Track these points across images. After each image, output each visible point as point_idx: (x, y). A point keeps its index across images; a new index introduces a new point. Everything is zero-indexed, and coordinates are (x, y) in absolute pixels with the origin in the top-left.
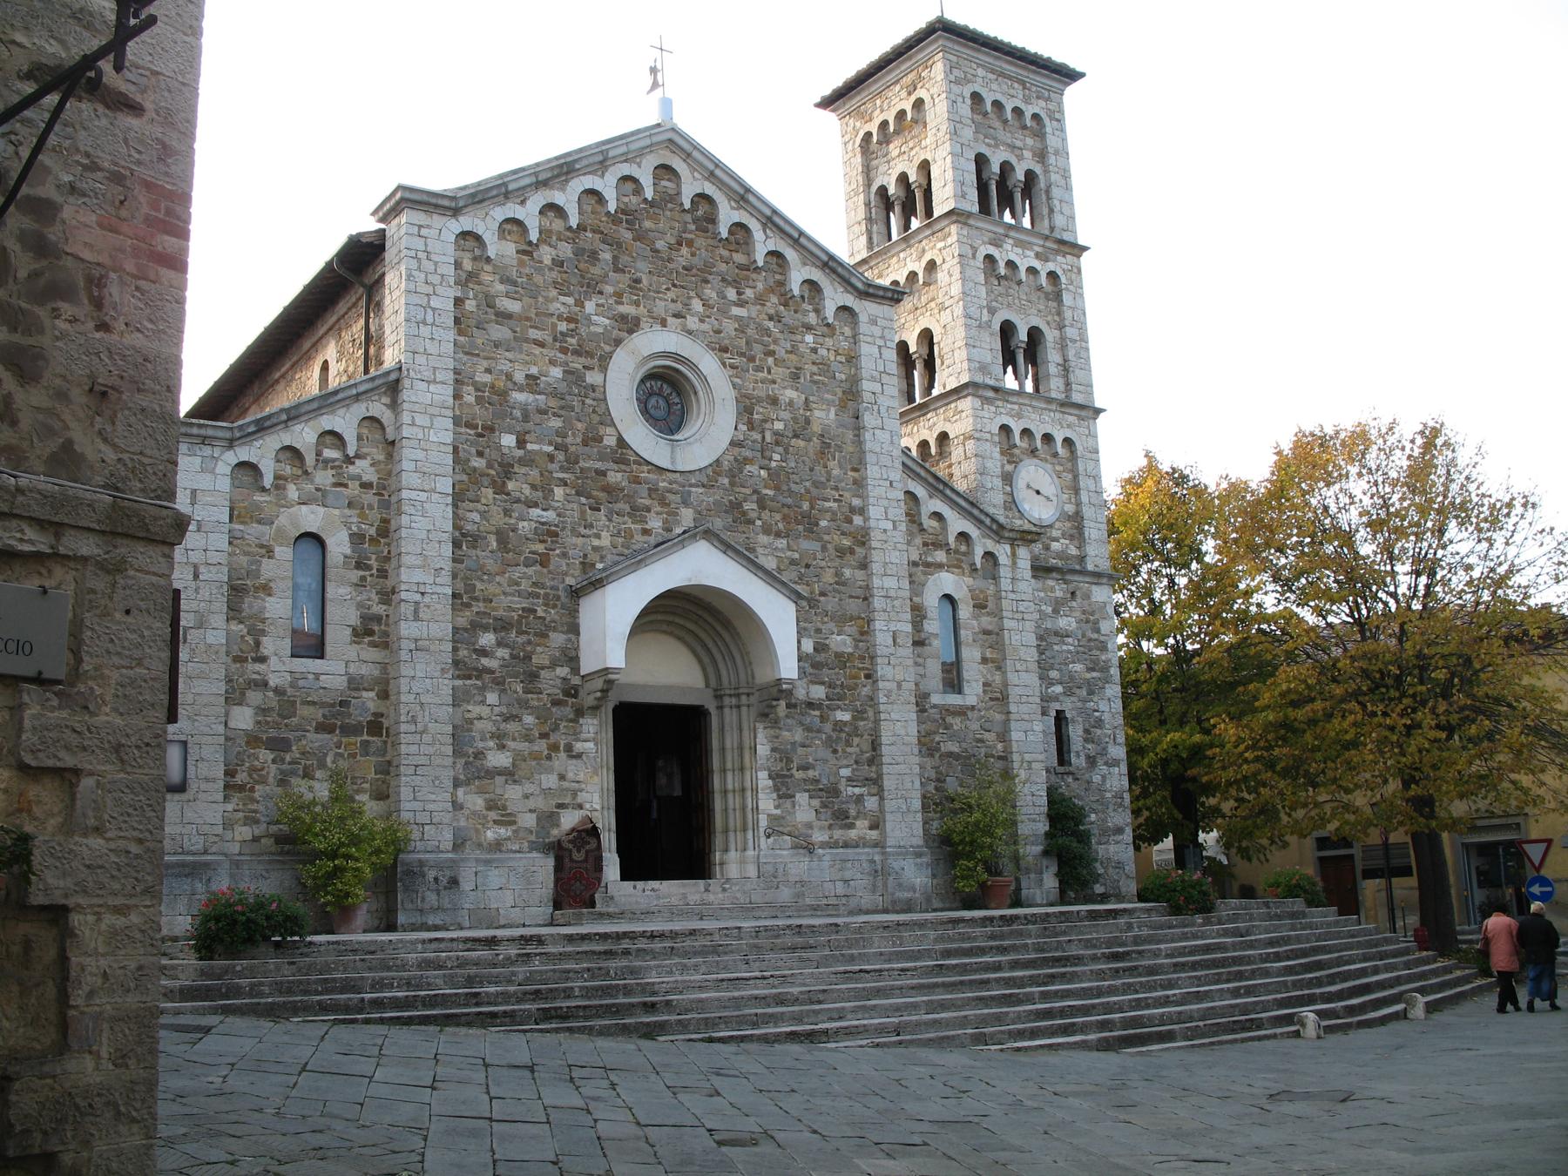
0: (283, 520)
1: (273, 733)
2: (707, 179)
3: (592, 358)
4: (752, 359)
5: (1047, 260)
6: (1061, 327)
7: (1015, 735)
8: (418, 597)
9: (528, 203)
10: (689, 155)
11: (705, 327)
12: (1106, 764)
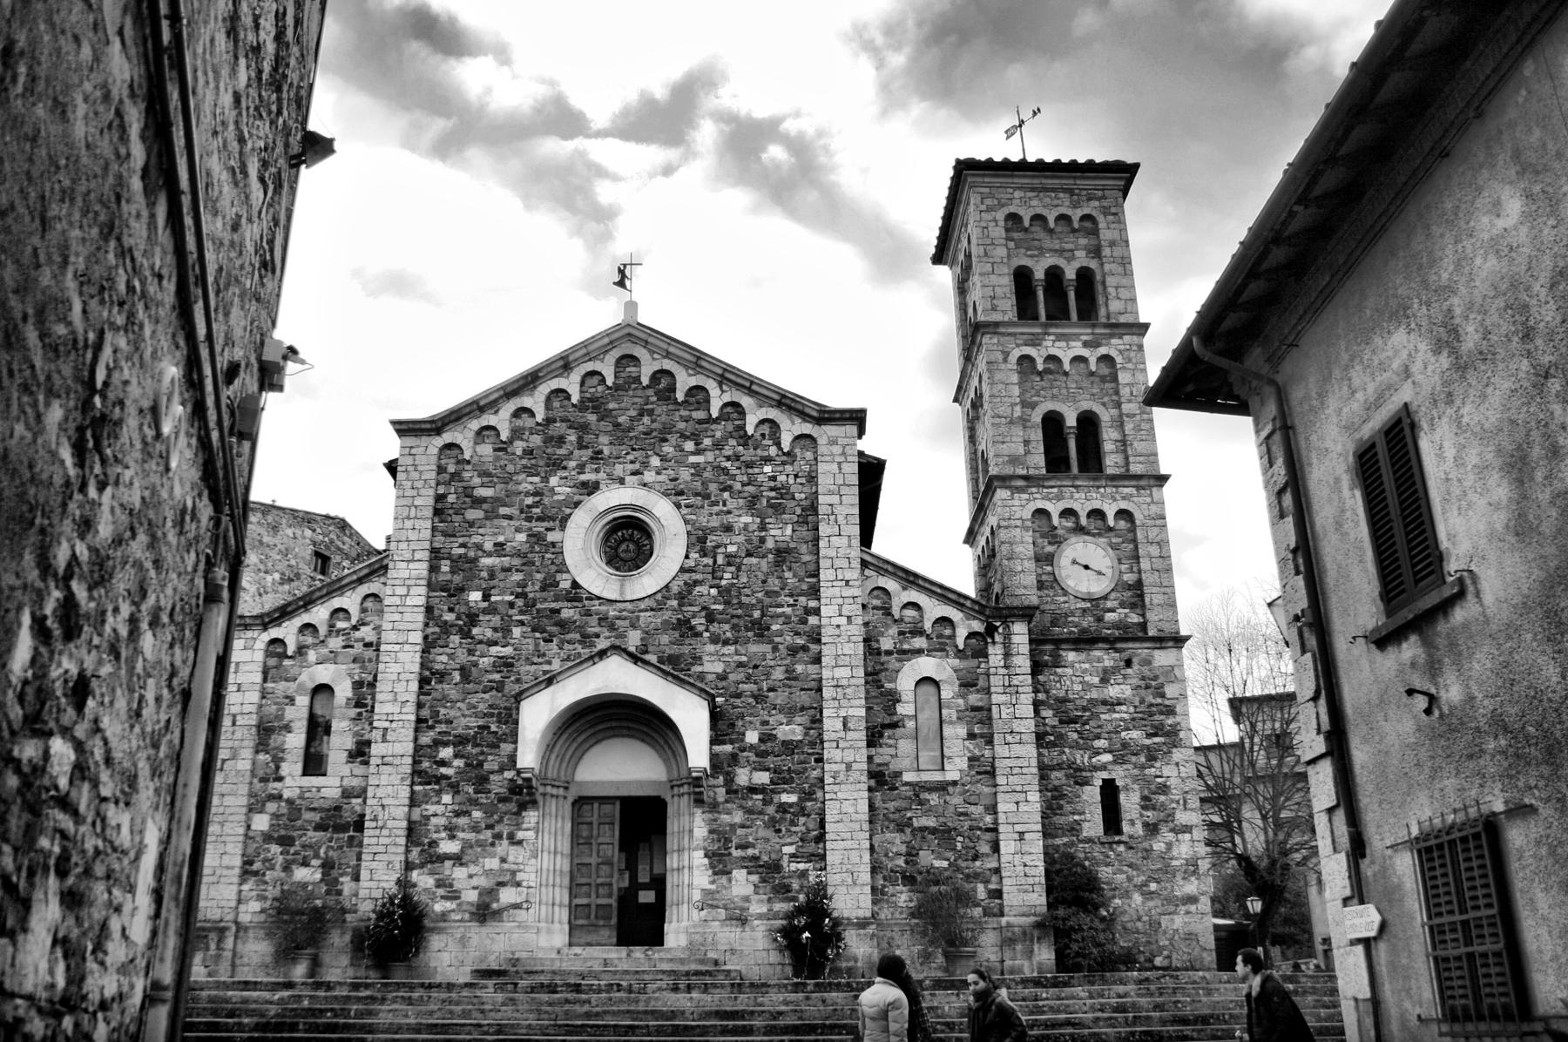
0: (304, 678)
1: (283, 832)
2: (665, 357)
3: (554, 520)
4: (707, 496)
5: (1098, 345)
7: (1001, 807)
8: (387, 724)
9: (501, 412)
10: (647, 342)
11: (660, 478)
12: (1172, 830)
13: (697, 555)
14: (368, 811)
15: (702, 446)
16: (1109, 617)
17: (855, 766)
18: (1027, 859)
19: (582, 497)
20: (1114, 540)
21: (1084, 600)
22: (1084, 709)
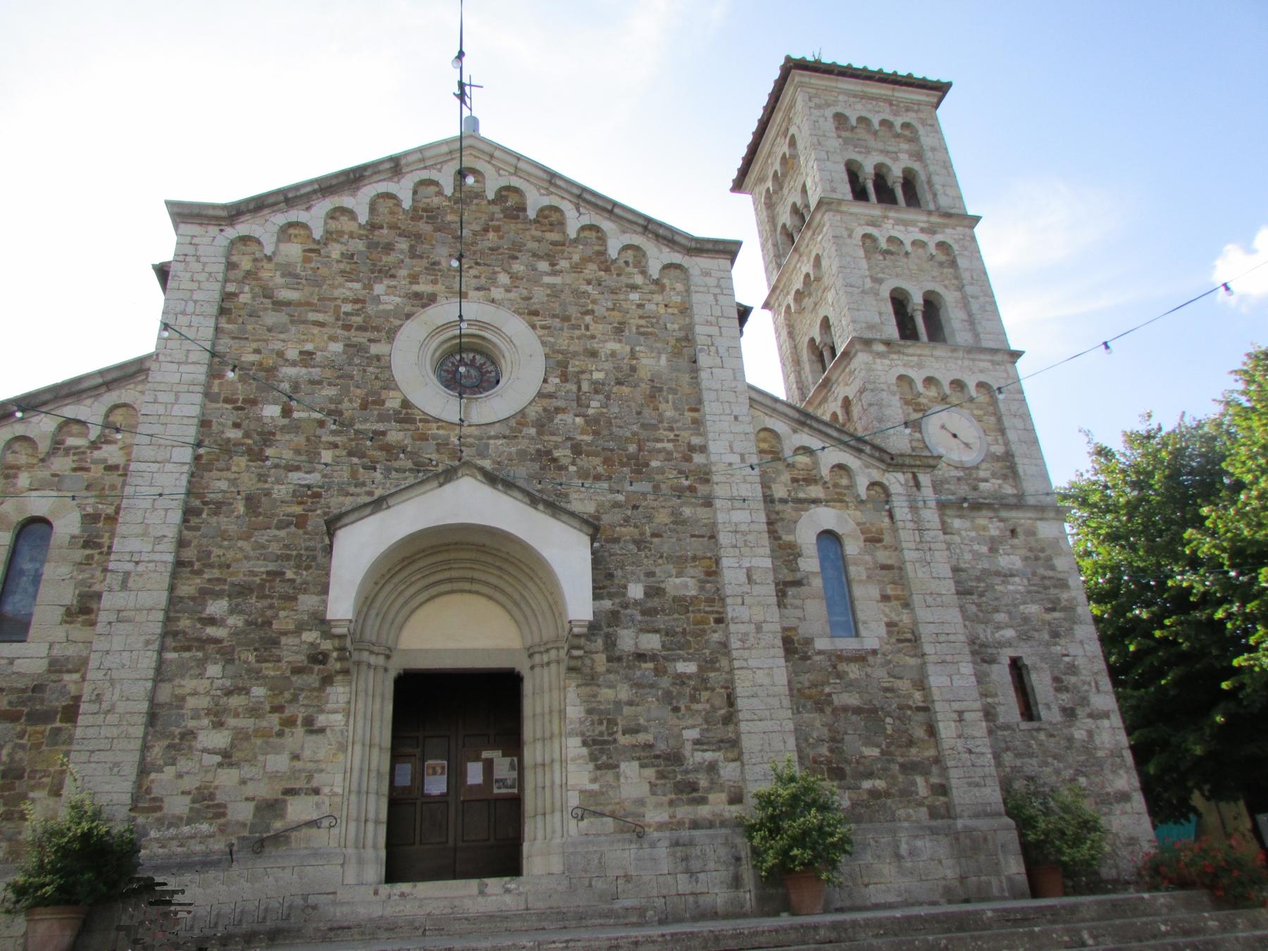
4: (566, 319)
5: (934, 233)
6: (961, 288)
8: (129, 567)
11: (512, 295)
12: (1090, 716)
13: (557, 380)
14: (87, 690)
15: (557, 267)
16: (983, 486)
17: (765, 627)
18: (970, 744)
19: (414, 309)
20: (976, 412)
21: (957, 468)
22: (978, 579)
